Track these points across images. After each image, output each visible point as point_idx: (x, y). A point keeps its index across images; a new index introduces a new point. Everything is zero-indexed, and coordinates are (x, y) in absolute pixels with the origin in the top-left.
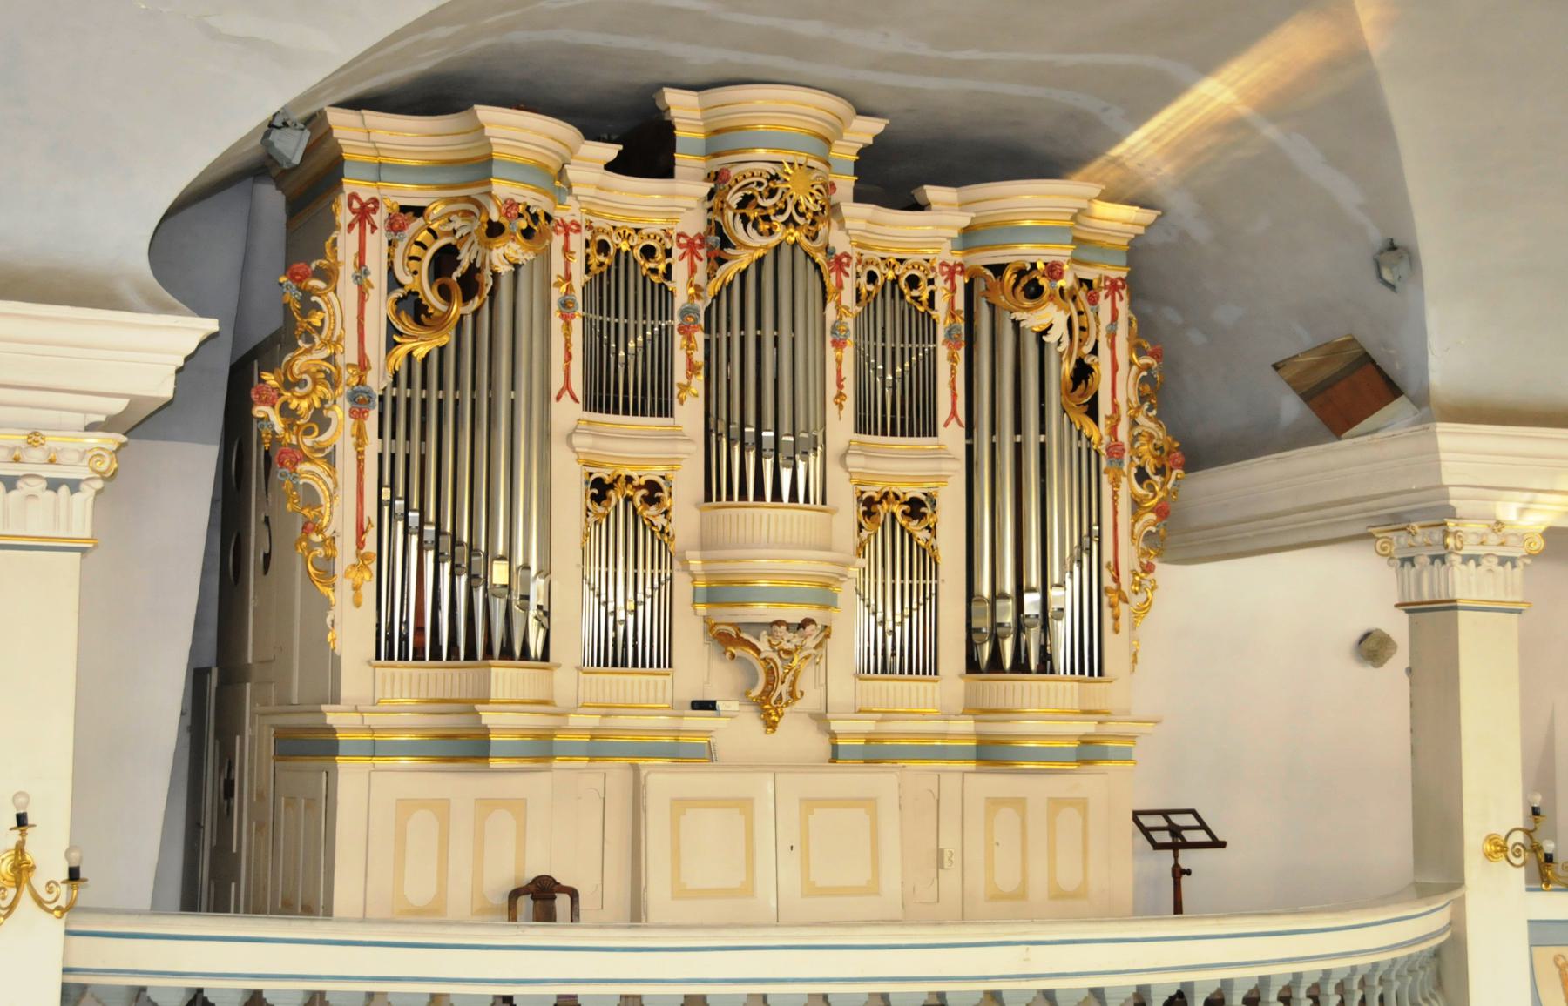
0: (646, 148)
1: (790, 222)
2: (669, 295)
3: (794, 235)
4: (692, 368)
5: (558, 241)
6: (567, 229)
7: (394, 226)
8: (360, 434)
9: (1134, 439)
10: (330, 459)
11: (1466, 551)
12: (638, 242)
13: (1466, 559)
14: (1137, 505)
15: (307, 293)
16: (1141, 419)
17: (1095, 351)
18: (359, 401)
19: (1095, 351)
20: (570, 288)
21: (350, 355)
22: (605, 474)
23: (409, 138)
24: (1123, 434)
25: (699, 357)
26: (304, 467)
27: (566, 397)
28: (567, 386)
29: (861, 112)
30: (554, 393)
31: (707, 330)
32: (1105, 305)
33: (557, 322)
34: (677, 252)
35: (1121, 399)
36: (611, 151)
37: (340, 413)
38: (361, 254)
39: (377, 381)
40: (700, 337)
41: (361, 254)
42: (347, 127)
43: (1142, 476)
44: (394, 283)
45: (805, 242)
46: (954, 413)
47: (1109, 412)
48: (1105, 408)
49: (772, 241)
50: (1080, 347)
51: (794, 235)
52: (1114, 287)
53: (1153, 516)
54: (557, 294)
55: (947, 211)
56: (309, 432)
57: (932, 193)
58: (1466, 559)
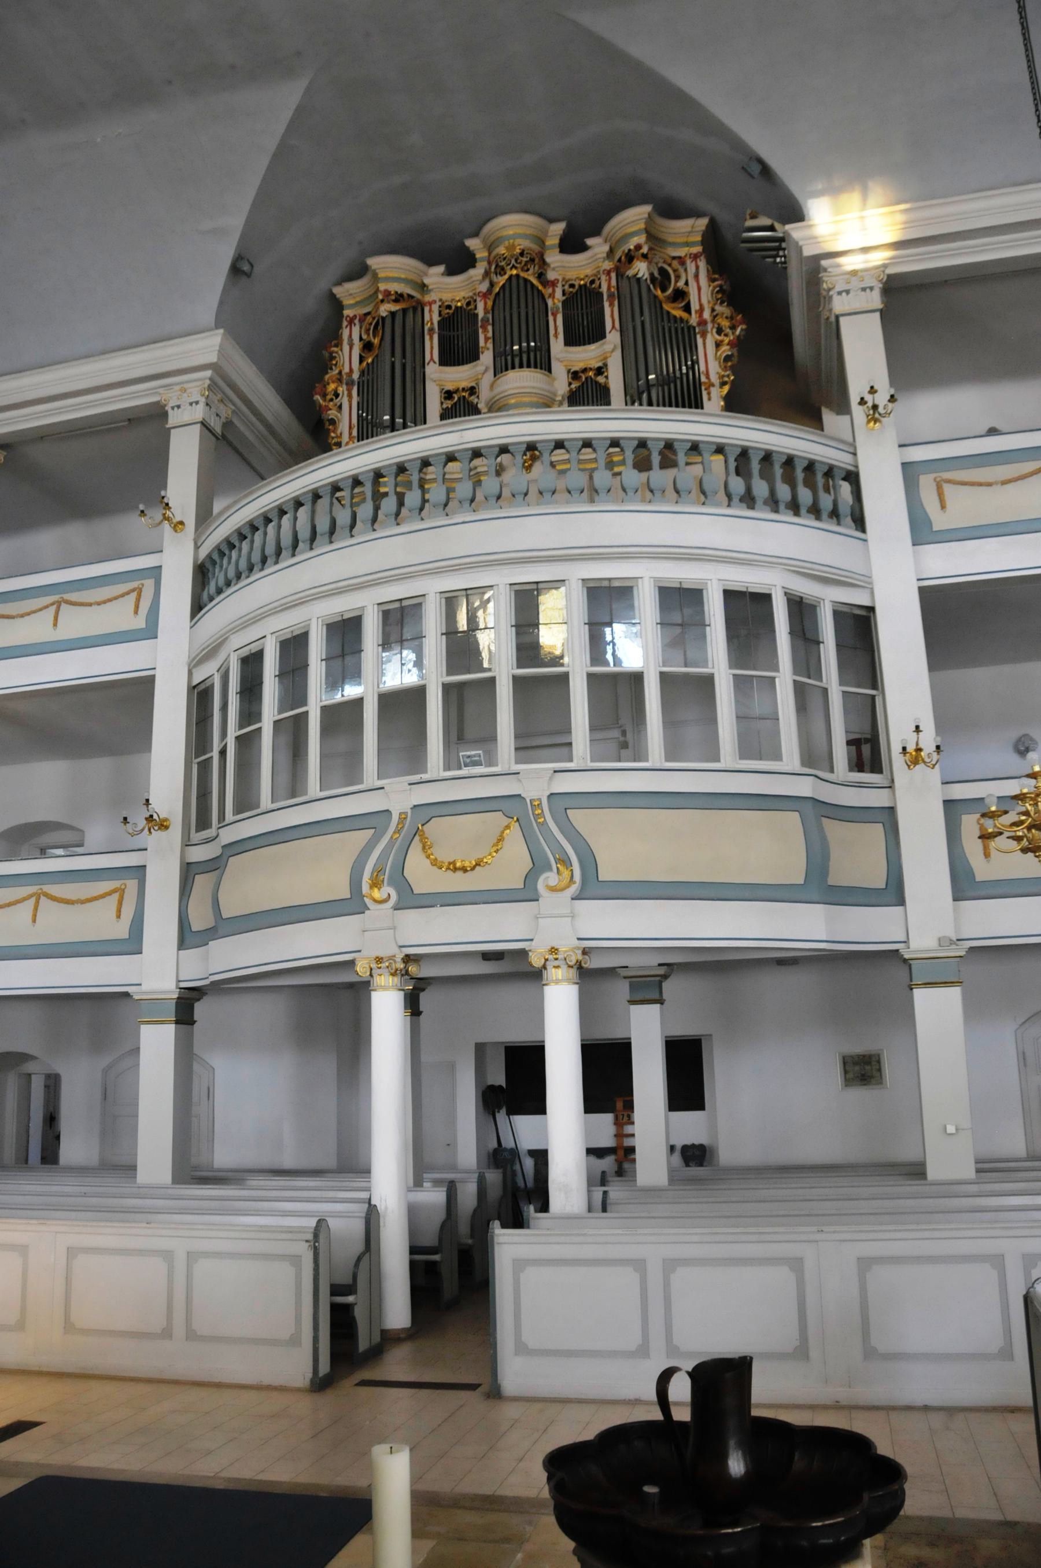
0: (460, 262)
1: (514, 267)
2: (477, 315)
3: (514, 272)
4: (486, 339)
5: (427, 309)
6: (430, 304)
7: (361, 321)
8: (350, 396)
9: (714, 318)
10: (340, 407)
11: (838, 289)
12: (464, 303)
13: (840, 293)
14: (718, 345)
15: (331, 353)
16: (718, 308)
17: (687, 283)
18: (350, 384)
19: (687, 283)
20: (432, 324)
21: (346, 369)
22: (450, 387)
23: (592, 355)
24: (707, 315)
25: (490, 334)
26: (330, 412)
27: (432, 363)
28: (432, 359)
29: (551, 221)
30: (427, 361)
31: (493, 325)
32: (691, 267)
33: (427, 338)
34: (478, 299)
35: (704, 301)
36: (441, 269)
37: (342, 389)
38: (350, 335)
39: (356, 376)
40: (490, 328)
41: (350, 335)
42: (337, 291)
43: (720, 331)
44: (361, 339)
45: (522, 274)
46: (613, 327)
47: (698, 308)
48: (695, 306)
49: (506, 277)
50: (676, 282)
51: (514, 272)
52: (695, 257)
53: (728, 347)
54: (426, 328)
55: (598, 246)
56: (331, 400)
57: (589, 242)
58: (840, 293)
